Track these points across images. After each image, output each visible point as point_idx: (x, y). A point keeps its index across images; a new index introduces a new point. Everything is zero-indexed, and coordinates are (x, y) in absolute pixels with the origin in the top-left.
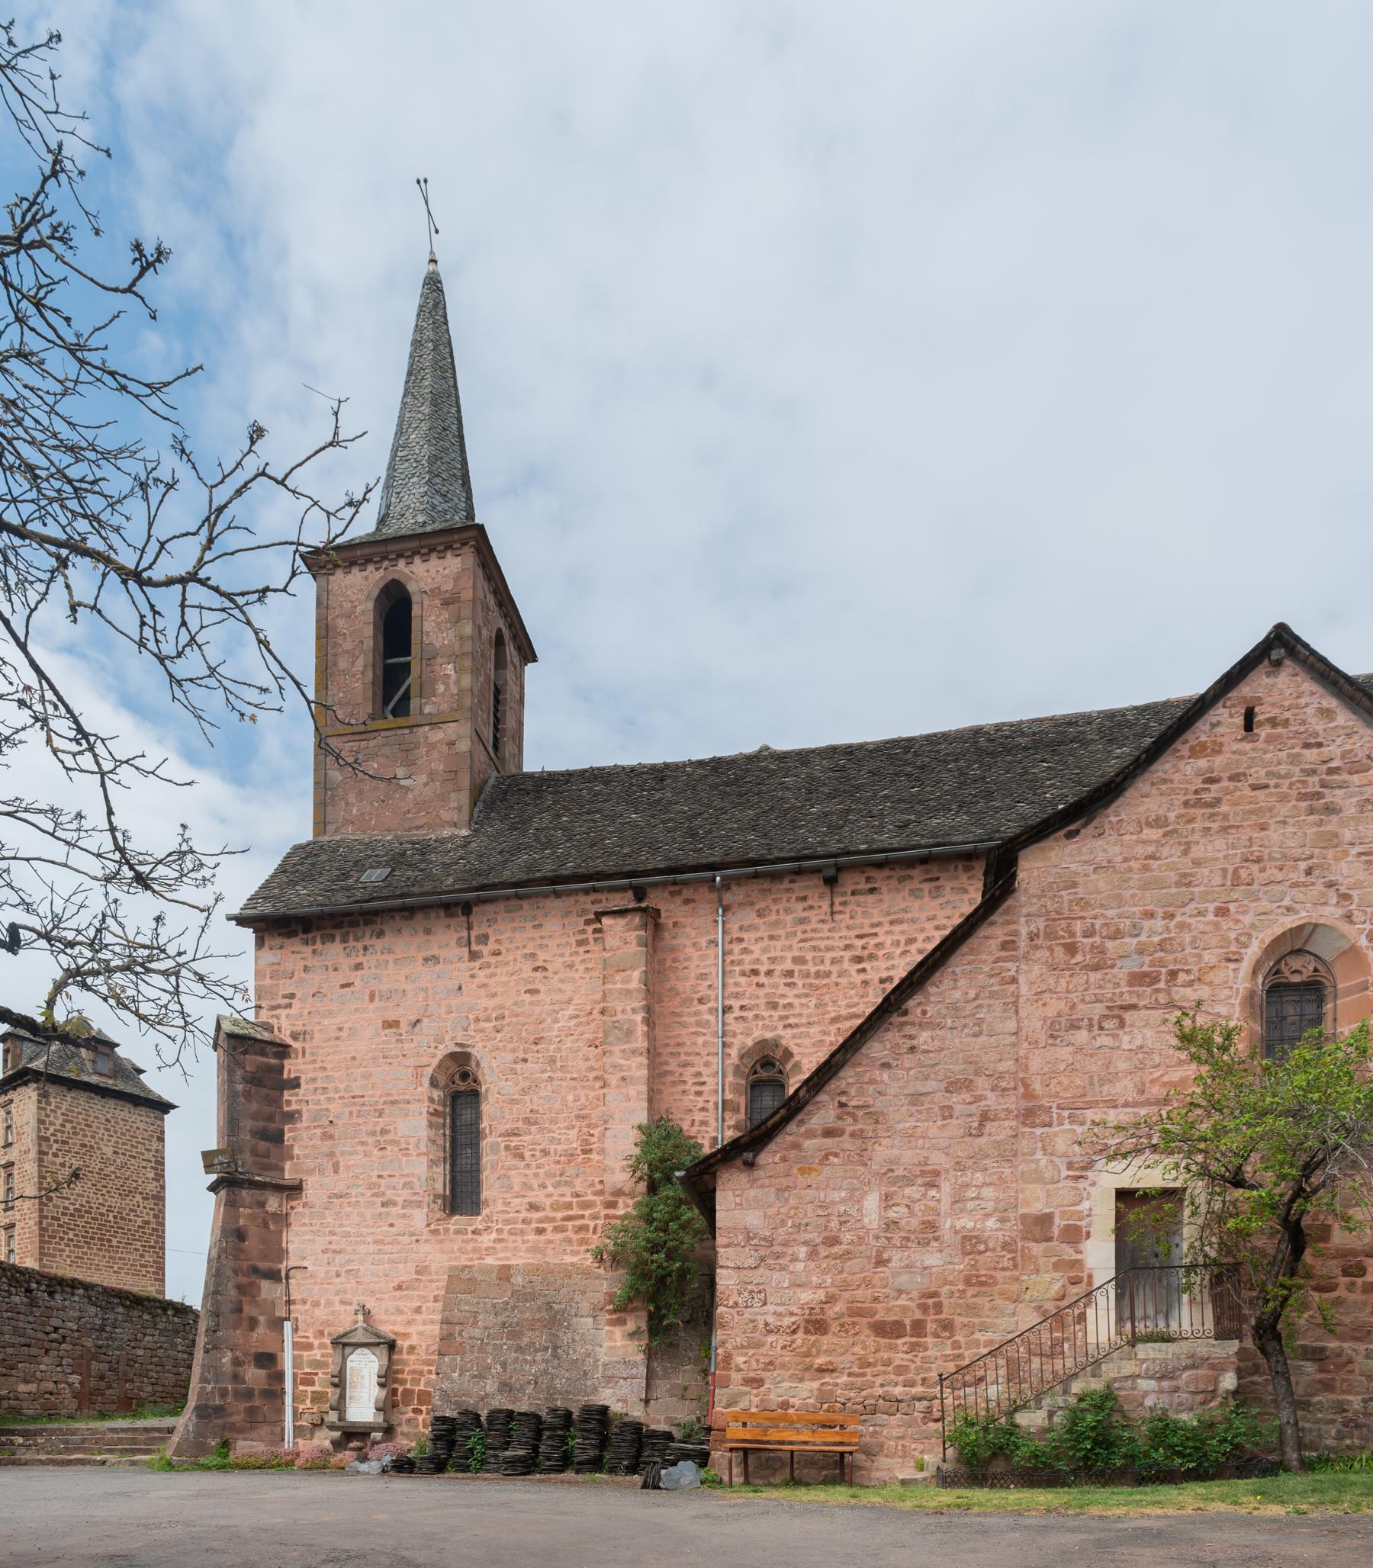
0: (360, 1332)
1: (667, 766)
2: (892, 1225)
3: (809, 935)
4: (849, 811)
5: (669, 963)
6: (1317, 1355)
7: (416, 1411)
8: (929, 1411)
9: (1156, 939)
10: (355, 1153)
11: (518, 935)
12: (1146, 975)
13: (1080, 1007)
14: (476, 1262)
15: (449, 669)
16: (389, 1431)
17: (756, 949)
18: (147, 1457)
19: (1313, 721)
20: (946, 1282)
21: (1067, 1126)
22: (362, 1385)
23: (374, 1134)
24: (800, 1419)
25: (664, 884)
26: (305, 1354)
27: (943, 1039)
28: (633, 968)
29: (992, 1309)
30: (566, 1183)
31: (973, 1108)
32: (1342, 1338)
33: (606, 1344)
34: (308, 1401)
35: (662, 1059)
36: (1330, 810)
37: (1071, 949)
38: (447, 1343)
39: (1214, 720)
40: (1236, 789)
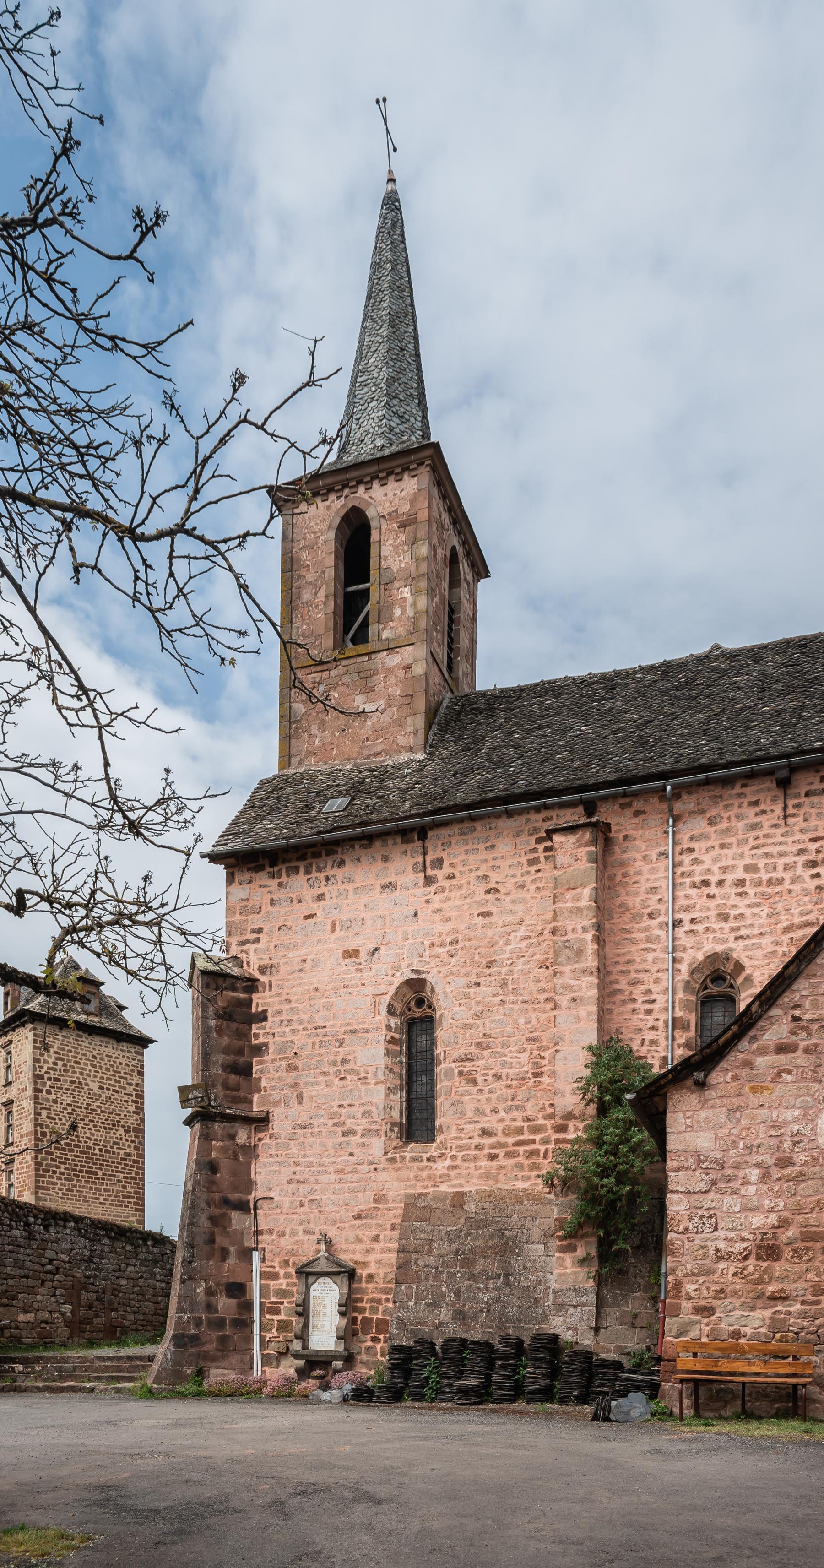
0: (322, 1261)
1: (617, 673)
3: (761, 841)
4: (803, 707)
5: (619, 878)
7: (375, 1340)
10: (316, 1084)
11: (471, 857)
14: (431, 1190)
15: (406, 592)
16: (349, 1359)
17: (707, 858)
22: (324, 1314)
23: (335, 1063)
25: (615, 797)
26: (272, 1283)
28: (584, 886)
30: (518, 1108)
33: (557, 1271)
34: (274, 1330)
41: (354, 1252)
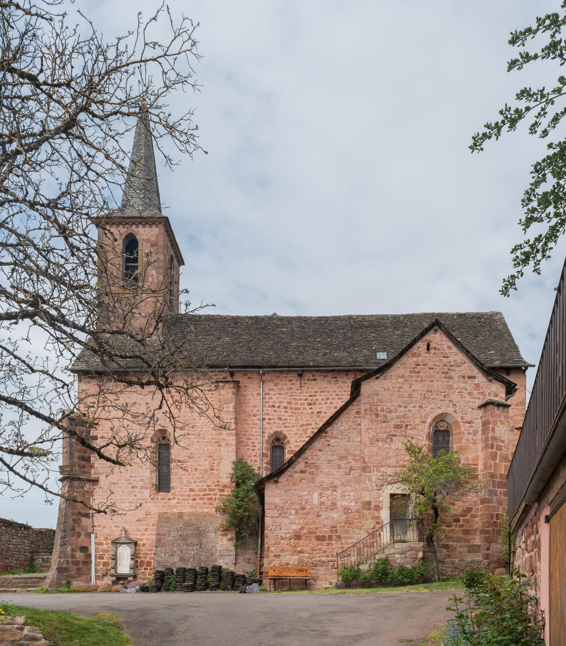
0: (123, 538)
1: (238, 317)
2: (323, 503)
3: (293, 394)
4: (306, 346)
5: (242, 400)
6: (446, 547)
7: (145, 569)
8: (333, 565)
9: (402, 414)
12: (399, 425)
13: (380, 434)
14: (169, 511)
15: (154, 272)
16: (135, 577)
17: (274, 397)
18: (34, 589)
19: (446, 349)
20: (339, 523)
21: (376, 473)
22: (124, 559)
24: (293, 568)
25: (241, 371)
26: (100, 547)
27: (338, 442)
28: (230, 403)
29: (353, 532)
30: (204, 481)
31: (347, 466)
32: (453, 541)
33: (220, 543)
34: (101, 566)
35: (240, 436)
36: (451, 378)
37: (377, 415)
38: (159, 543)
39: (419, 346)
40: (425, 368)
41: (137, 535)
